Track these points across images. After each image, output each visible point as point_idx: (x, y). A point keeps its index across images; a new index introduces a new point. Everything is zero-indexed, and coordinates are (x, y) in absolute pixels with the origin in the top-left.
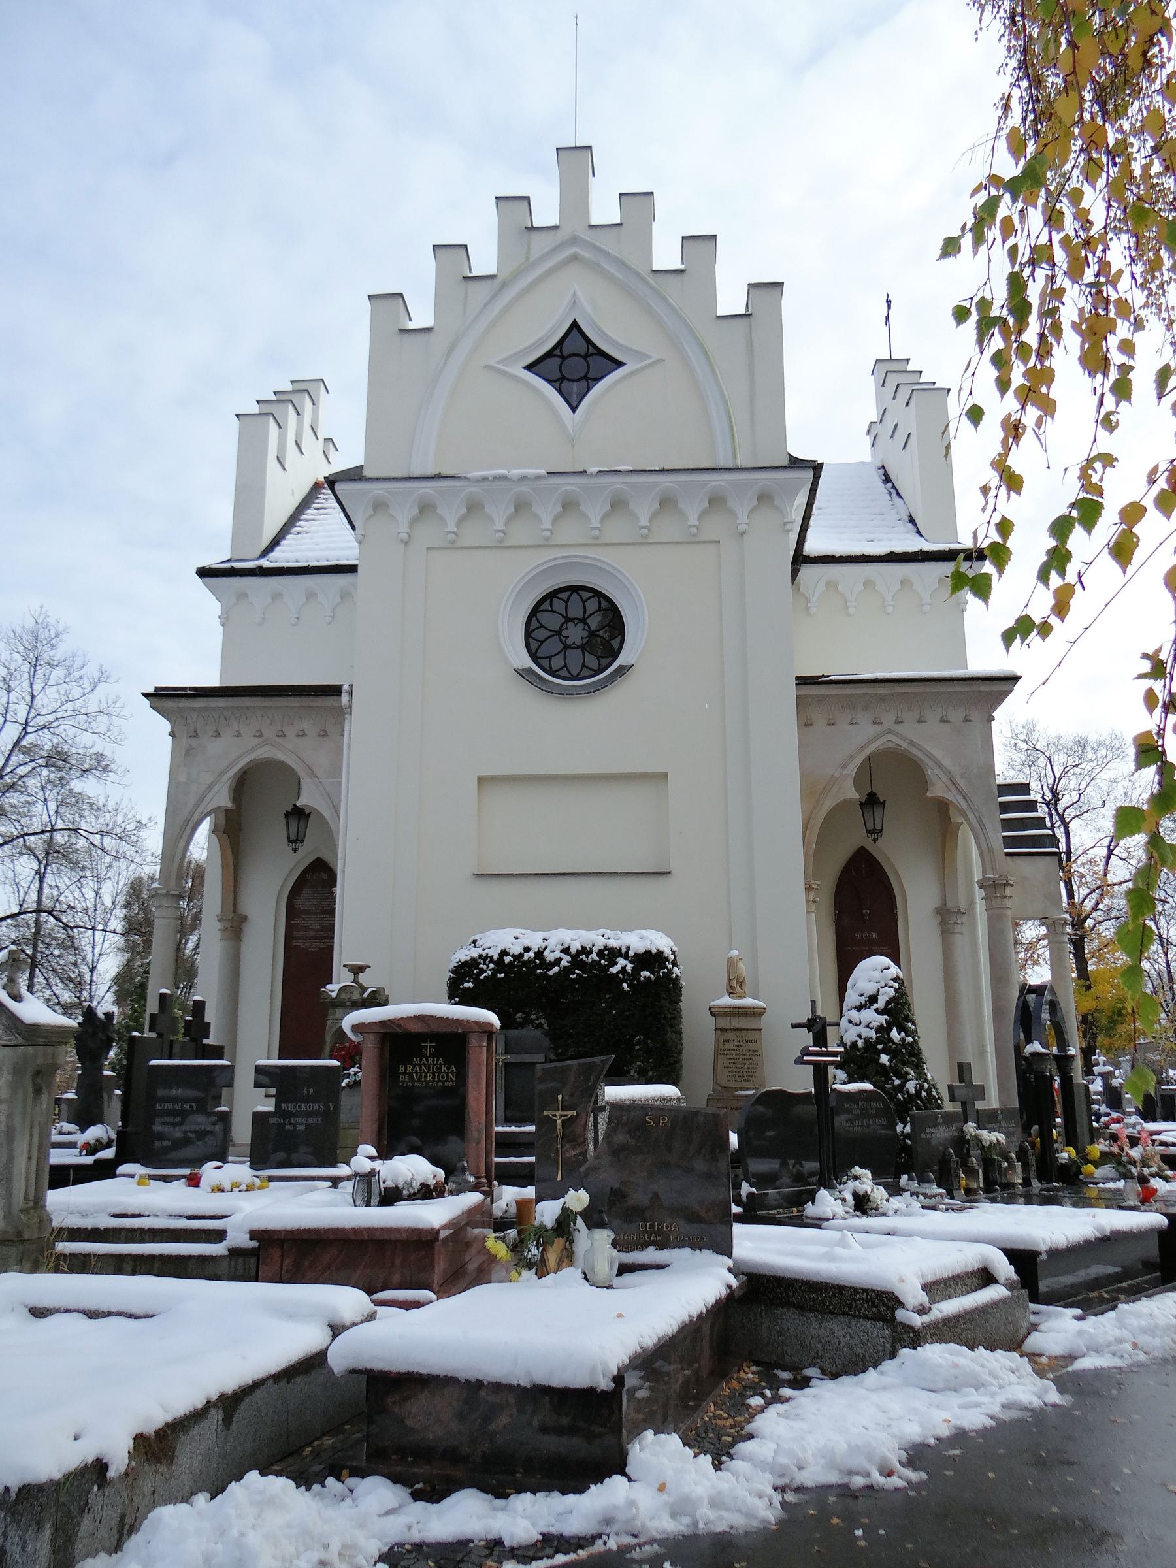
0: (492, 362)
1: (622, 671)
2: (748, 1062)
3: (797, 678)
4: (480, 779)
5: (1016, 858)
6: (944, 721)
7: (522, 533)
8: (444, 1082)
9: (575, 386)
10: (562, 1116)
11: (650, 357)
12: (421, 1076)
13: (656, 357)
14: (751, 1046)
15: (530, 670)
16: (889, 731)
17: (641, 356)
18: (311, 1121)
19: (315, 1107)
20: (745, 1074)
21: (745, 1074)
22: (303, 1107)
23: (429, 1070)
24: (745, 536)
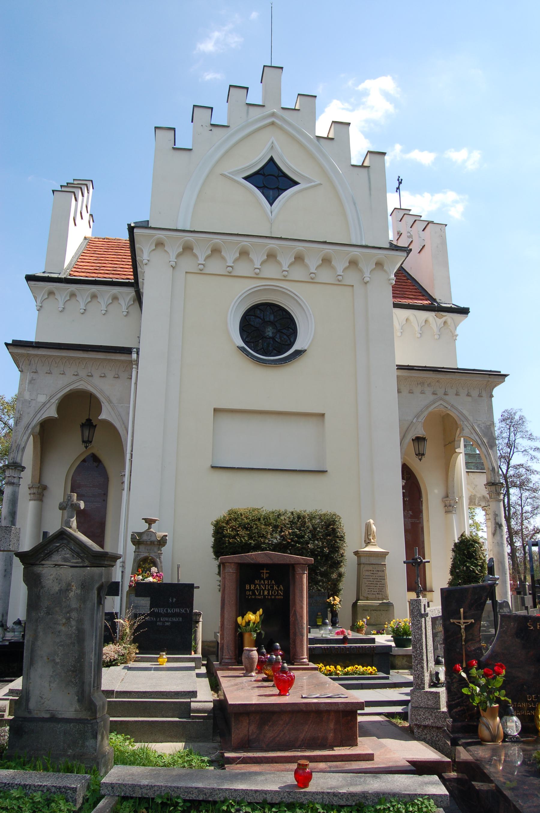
0: (226, 173)
1: (299, 353)
2: (379, 583)
3: (397, 366)
4: (215, 410)
5: (473, 473)
6: (468, 395)
7: (243, 269)
8: (275, 596)
9: (271, 192)
10: (464, 623)
11: (315, 182)
12: (260, 592)
13: (318, 182)
14: (380, 573)
15: (243, 348)
16: (441, 399)
17: (309, 180)
18: (174, 619)
19: (177, 610)
20: (377, 590)
21: (377, 590)
22: (169, 611)
23: (265, 588)
24: (368, 284)
